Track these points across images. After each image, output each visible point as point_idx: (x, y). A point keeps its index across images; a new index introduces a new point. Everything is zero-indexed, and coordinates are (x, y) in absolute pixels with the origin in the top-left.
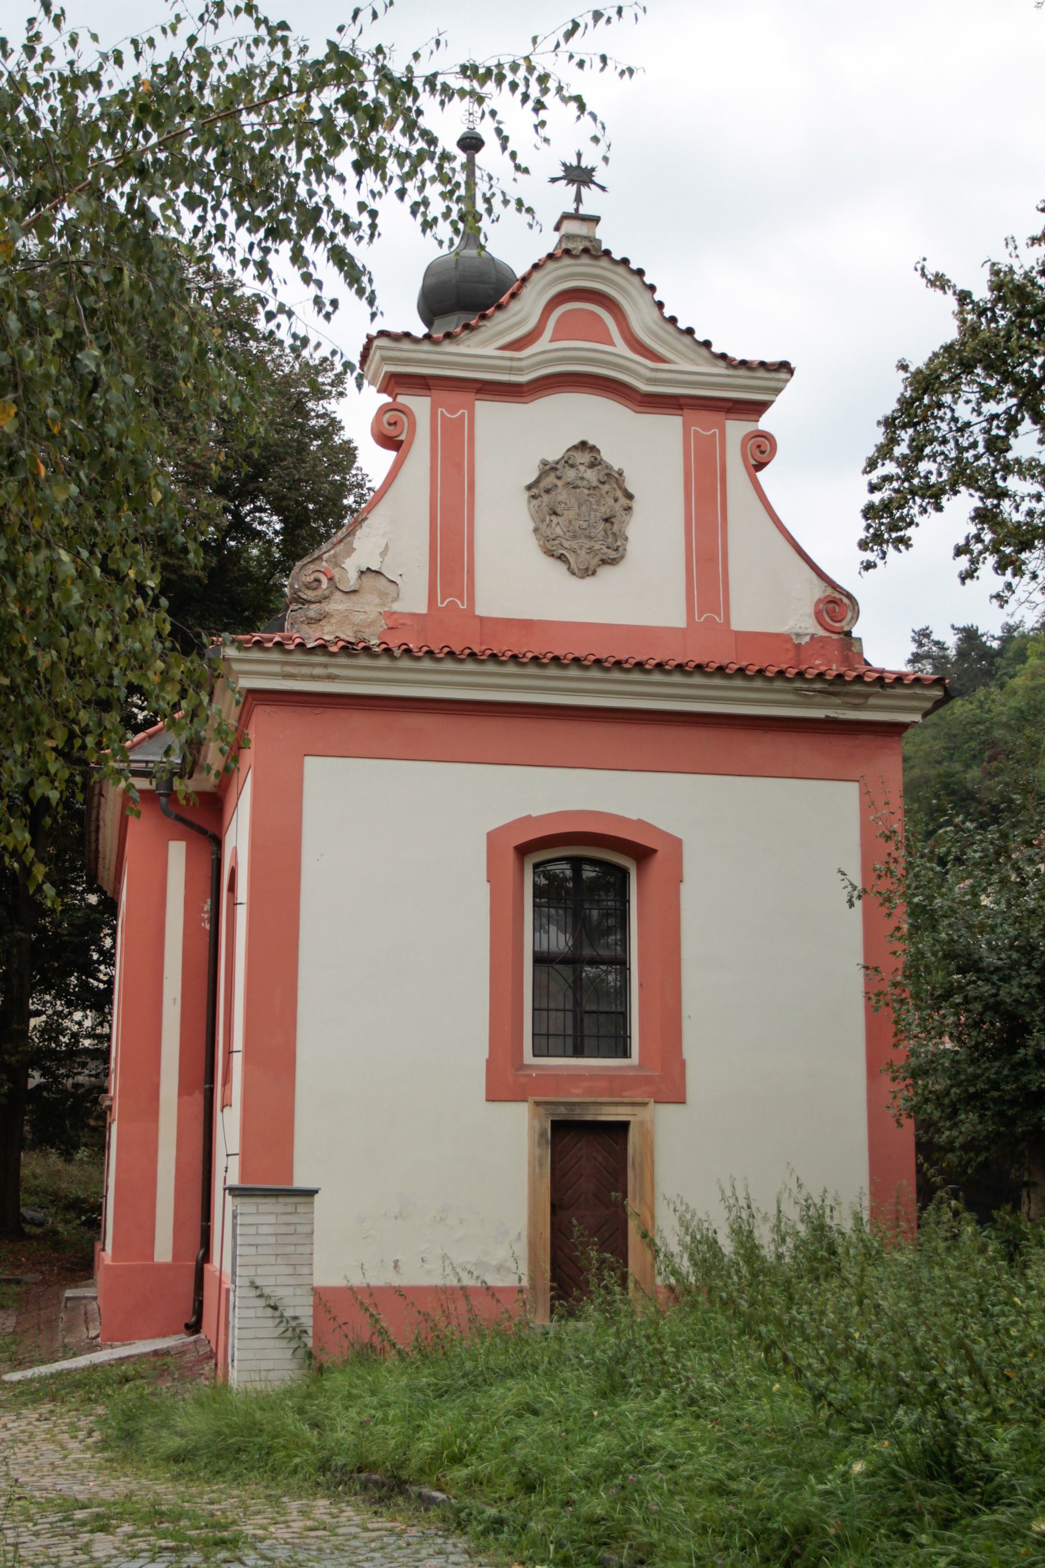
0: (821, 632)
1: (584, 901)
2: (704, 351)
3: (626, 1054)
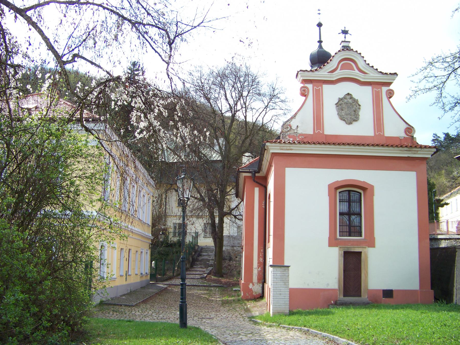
0: (406, 136)
2: (376, 71)
3: (361, 236)
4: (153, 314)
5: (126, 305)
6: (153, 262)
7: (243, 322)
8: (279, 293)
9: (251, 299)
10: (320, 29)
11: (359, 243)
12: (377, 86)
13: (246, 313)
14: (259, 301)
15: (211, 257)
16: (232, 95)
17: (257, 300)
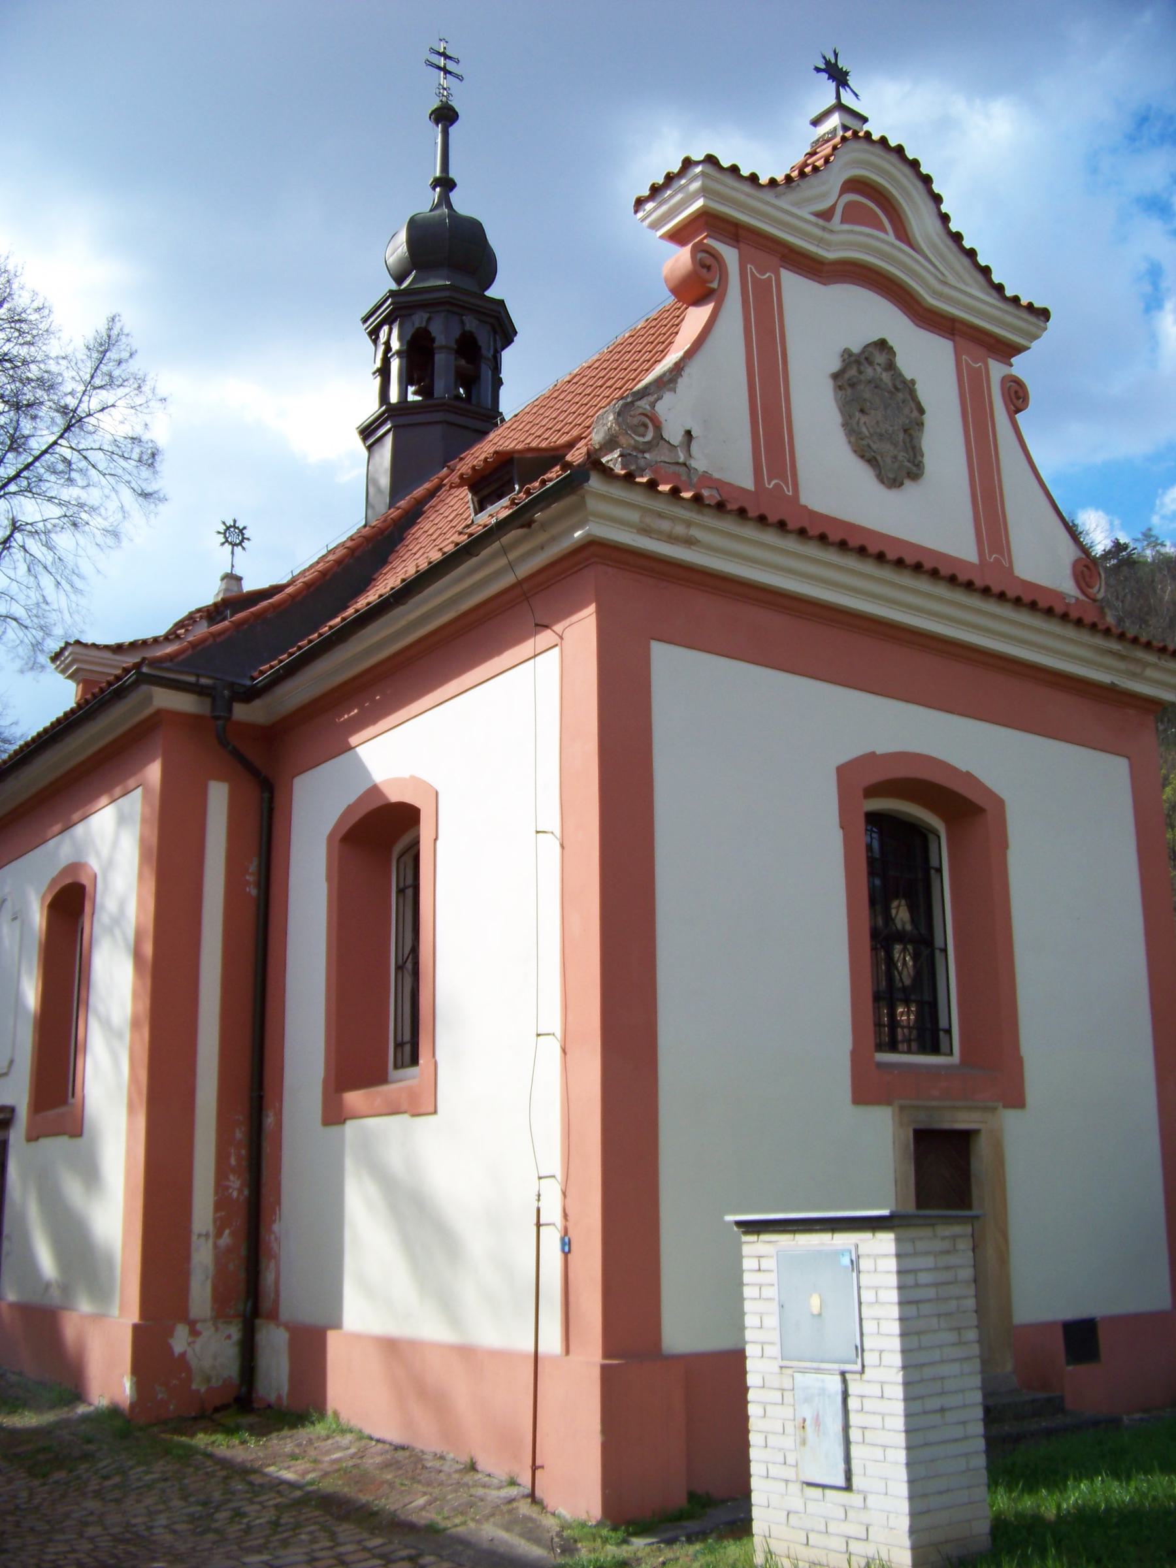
3: (951, 1053)
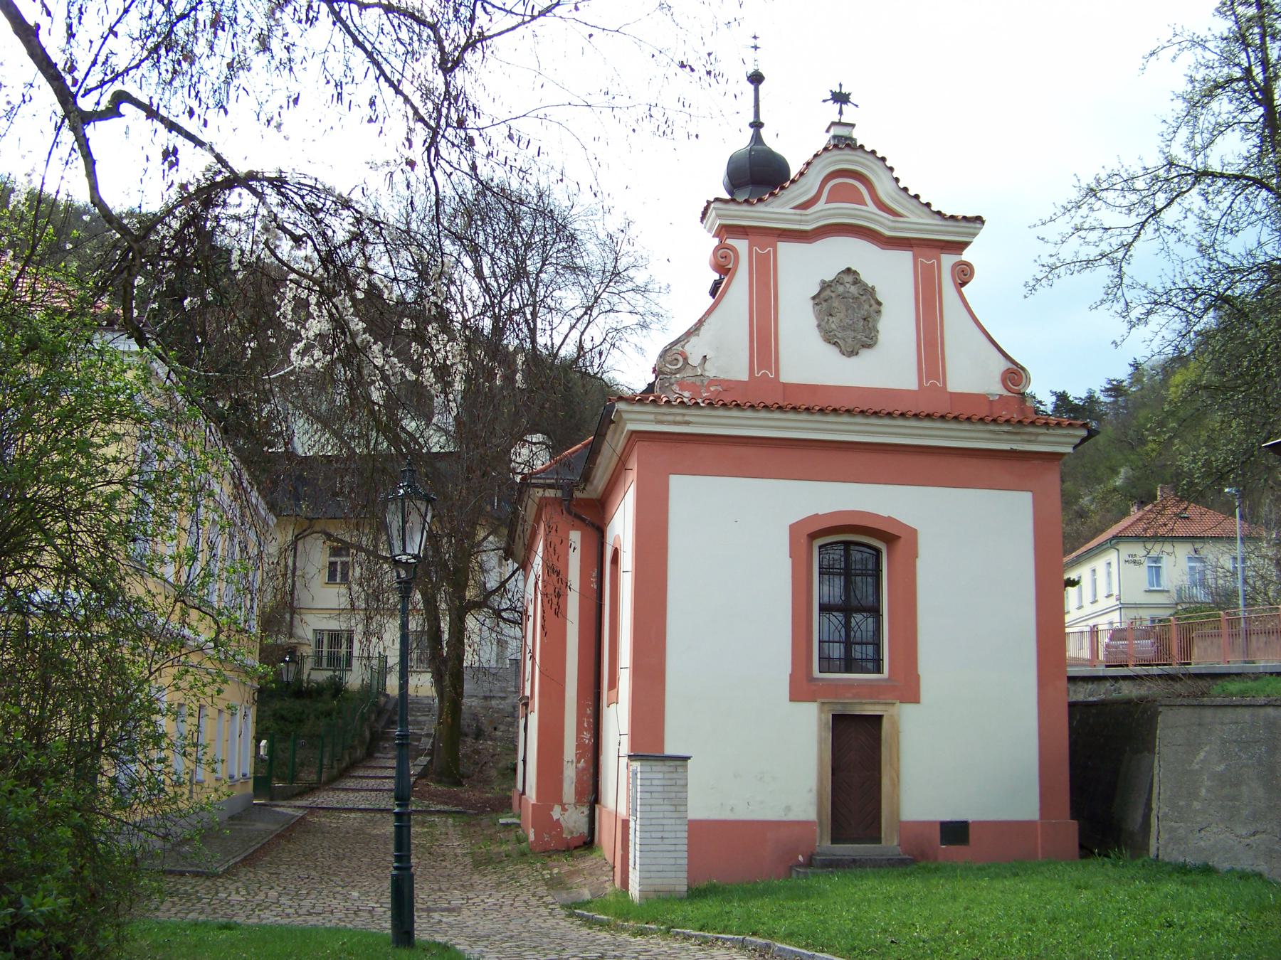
0: (1005, 393)
1: (853, 581)
2: (925, 209)
3: (879, 670)
4: (283, 900)
5: (197, 874)
6: (264, 742)
7: (551, 922)
8: (659, 835)
9: (557, 851)
10: (756, 91)
11: (874, 691)
12: (927, 251)
13: (552, 892)
14: (581, 856)
15: (426, 727)
16: (497, 261)
17: (576, 853)
